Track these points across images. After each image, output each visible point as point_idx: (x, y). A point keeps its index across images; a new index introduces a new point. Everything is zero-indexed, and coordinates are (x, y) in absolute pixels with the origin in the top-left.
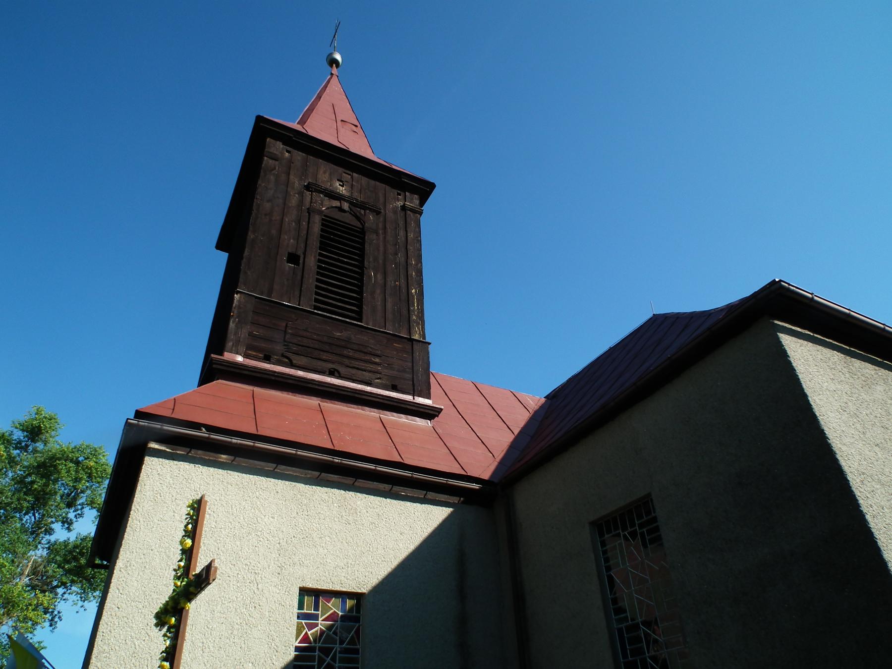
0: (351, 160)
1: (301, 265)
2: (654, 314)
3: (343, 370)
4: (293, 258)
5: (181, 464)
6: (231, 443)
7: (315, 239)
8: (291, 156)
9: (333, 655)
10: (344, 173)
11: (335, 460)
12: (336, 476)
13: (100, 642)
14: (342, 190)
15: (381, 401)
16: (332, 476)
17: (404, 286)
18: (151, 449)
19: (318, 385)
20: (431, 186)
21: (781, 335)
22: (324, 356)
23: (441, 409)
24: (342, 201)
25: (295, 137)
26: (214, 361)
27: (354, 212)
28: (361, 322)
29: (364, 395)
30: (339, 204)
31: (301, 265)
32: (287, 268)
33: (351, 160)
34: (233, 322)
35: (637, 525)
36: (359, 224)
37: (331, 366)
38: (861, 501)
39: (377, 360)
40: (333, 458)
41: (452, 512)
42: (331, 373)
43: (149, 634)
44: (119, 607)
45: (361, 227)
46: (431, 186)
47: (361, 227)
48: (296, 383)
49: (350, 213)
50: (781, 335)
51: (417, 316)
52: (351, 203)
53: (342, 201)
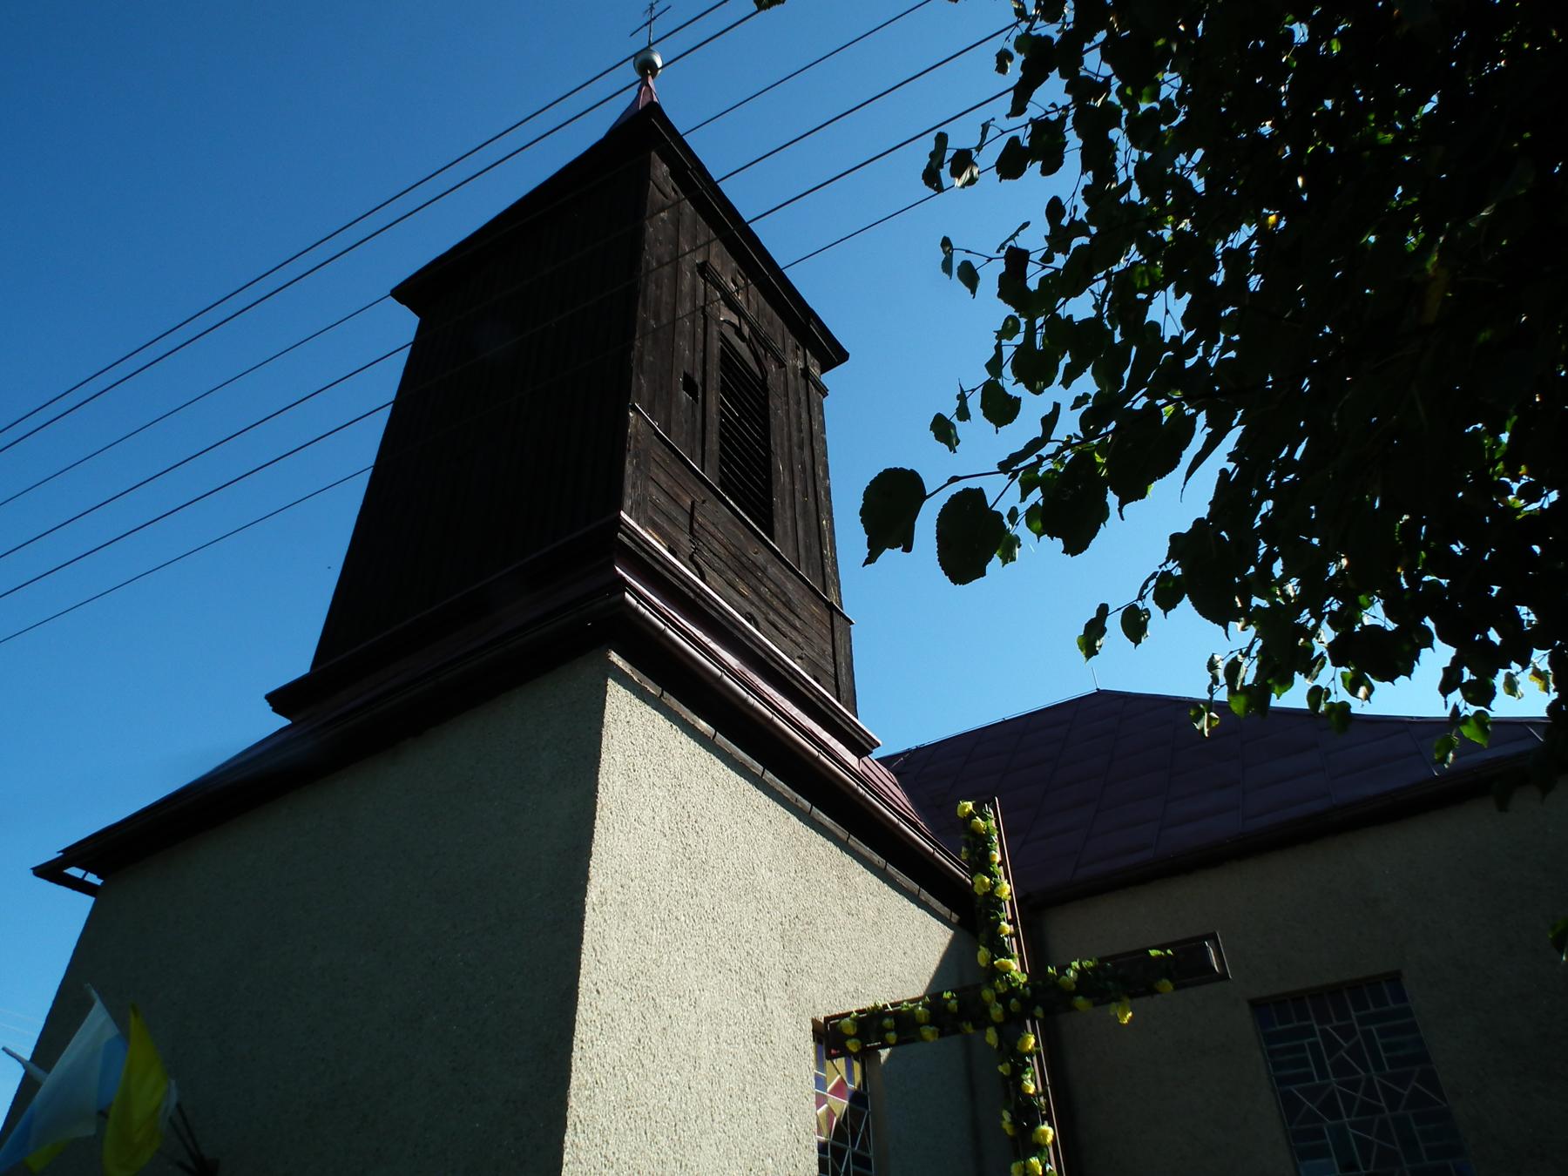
2: (1098, 689)
6: (745, 701)
7: (715, 367)
9: (846, 1167)
10: (739, 272)
11: (859, 788)
12: (828, 819)
13: (580, 1064)
15: (814, 699)
16: (825, 816)
18: (1470, 695)
20: (843, 356)
23: (879, 745)
26: (622, 526)
27: (755, 349)
35: (1318, 1033)
38: (580, 1007)
39: (798, 623)
40: (858, 785)
43: (643, 1062)
44: (600, 990)
46: (843, 356)
48: (720, 619)
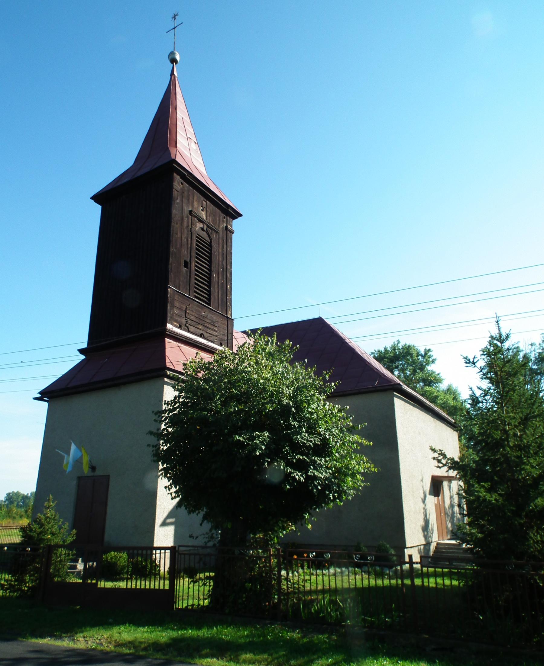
0: (209, 194)
1: (189, 268)
3: (206, 335)
4: (186, 265)
5: (166, 394)
8: (183, 187)
14: (203, 215)
17: (225, 282)
19: (190, 340)
21: (175, 174)
22: (200, 327)
24: (204, 224)
25: (188, 176)
28: (210, 306)
29: (178, 335)
30: (202, 225)
31: (189, 268)
32: (184, 271)
33: (209, 194)
34: (169, 306)
36: (208, 239)
37: (201, 332)
41: (83, 360)
42: (201, 336)
45: (210, 242)
47: (210, 242)
49: (206, 232)
50: (175, 174)
51: (229, 303)
52: (208, 226)
53: (204, 224)
